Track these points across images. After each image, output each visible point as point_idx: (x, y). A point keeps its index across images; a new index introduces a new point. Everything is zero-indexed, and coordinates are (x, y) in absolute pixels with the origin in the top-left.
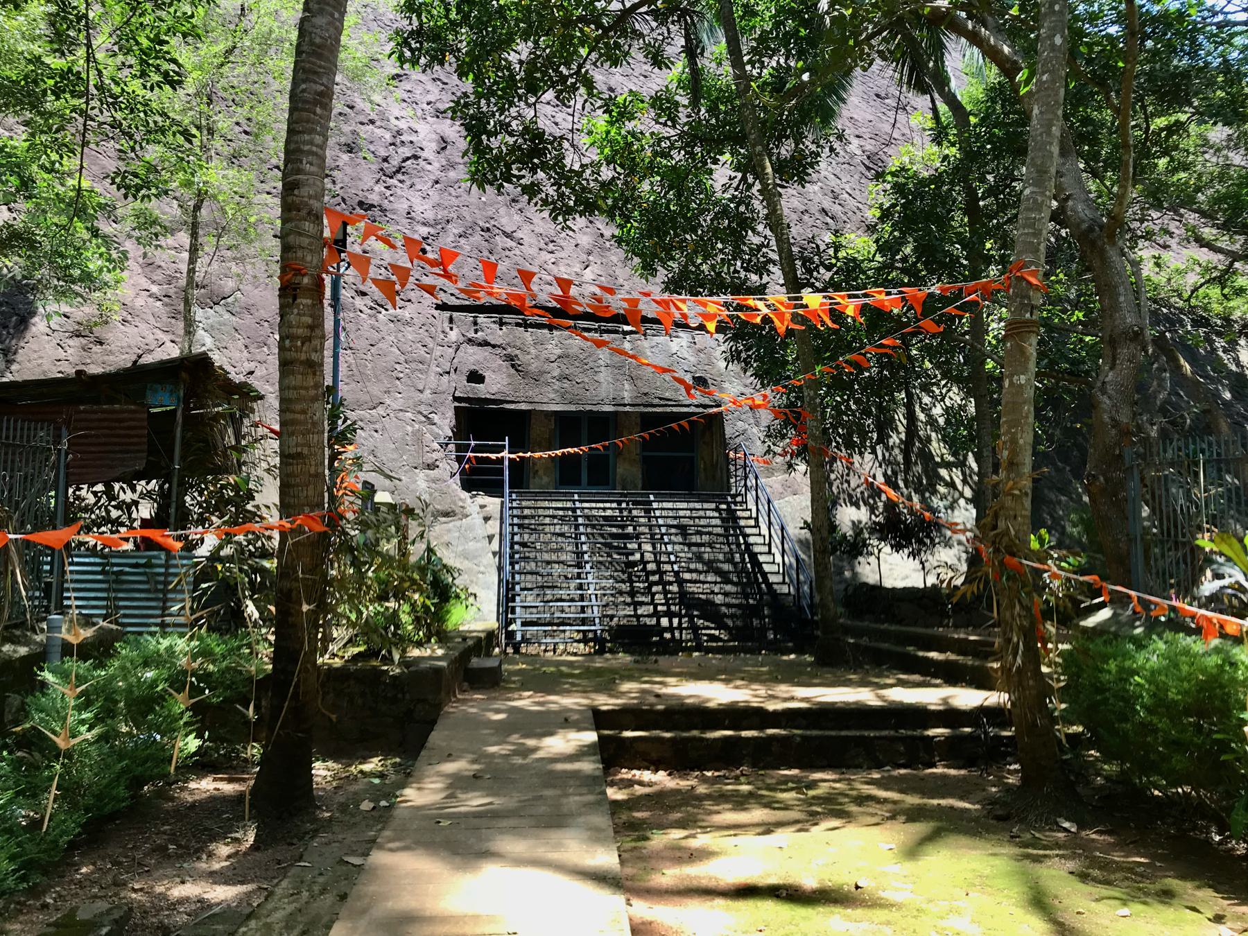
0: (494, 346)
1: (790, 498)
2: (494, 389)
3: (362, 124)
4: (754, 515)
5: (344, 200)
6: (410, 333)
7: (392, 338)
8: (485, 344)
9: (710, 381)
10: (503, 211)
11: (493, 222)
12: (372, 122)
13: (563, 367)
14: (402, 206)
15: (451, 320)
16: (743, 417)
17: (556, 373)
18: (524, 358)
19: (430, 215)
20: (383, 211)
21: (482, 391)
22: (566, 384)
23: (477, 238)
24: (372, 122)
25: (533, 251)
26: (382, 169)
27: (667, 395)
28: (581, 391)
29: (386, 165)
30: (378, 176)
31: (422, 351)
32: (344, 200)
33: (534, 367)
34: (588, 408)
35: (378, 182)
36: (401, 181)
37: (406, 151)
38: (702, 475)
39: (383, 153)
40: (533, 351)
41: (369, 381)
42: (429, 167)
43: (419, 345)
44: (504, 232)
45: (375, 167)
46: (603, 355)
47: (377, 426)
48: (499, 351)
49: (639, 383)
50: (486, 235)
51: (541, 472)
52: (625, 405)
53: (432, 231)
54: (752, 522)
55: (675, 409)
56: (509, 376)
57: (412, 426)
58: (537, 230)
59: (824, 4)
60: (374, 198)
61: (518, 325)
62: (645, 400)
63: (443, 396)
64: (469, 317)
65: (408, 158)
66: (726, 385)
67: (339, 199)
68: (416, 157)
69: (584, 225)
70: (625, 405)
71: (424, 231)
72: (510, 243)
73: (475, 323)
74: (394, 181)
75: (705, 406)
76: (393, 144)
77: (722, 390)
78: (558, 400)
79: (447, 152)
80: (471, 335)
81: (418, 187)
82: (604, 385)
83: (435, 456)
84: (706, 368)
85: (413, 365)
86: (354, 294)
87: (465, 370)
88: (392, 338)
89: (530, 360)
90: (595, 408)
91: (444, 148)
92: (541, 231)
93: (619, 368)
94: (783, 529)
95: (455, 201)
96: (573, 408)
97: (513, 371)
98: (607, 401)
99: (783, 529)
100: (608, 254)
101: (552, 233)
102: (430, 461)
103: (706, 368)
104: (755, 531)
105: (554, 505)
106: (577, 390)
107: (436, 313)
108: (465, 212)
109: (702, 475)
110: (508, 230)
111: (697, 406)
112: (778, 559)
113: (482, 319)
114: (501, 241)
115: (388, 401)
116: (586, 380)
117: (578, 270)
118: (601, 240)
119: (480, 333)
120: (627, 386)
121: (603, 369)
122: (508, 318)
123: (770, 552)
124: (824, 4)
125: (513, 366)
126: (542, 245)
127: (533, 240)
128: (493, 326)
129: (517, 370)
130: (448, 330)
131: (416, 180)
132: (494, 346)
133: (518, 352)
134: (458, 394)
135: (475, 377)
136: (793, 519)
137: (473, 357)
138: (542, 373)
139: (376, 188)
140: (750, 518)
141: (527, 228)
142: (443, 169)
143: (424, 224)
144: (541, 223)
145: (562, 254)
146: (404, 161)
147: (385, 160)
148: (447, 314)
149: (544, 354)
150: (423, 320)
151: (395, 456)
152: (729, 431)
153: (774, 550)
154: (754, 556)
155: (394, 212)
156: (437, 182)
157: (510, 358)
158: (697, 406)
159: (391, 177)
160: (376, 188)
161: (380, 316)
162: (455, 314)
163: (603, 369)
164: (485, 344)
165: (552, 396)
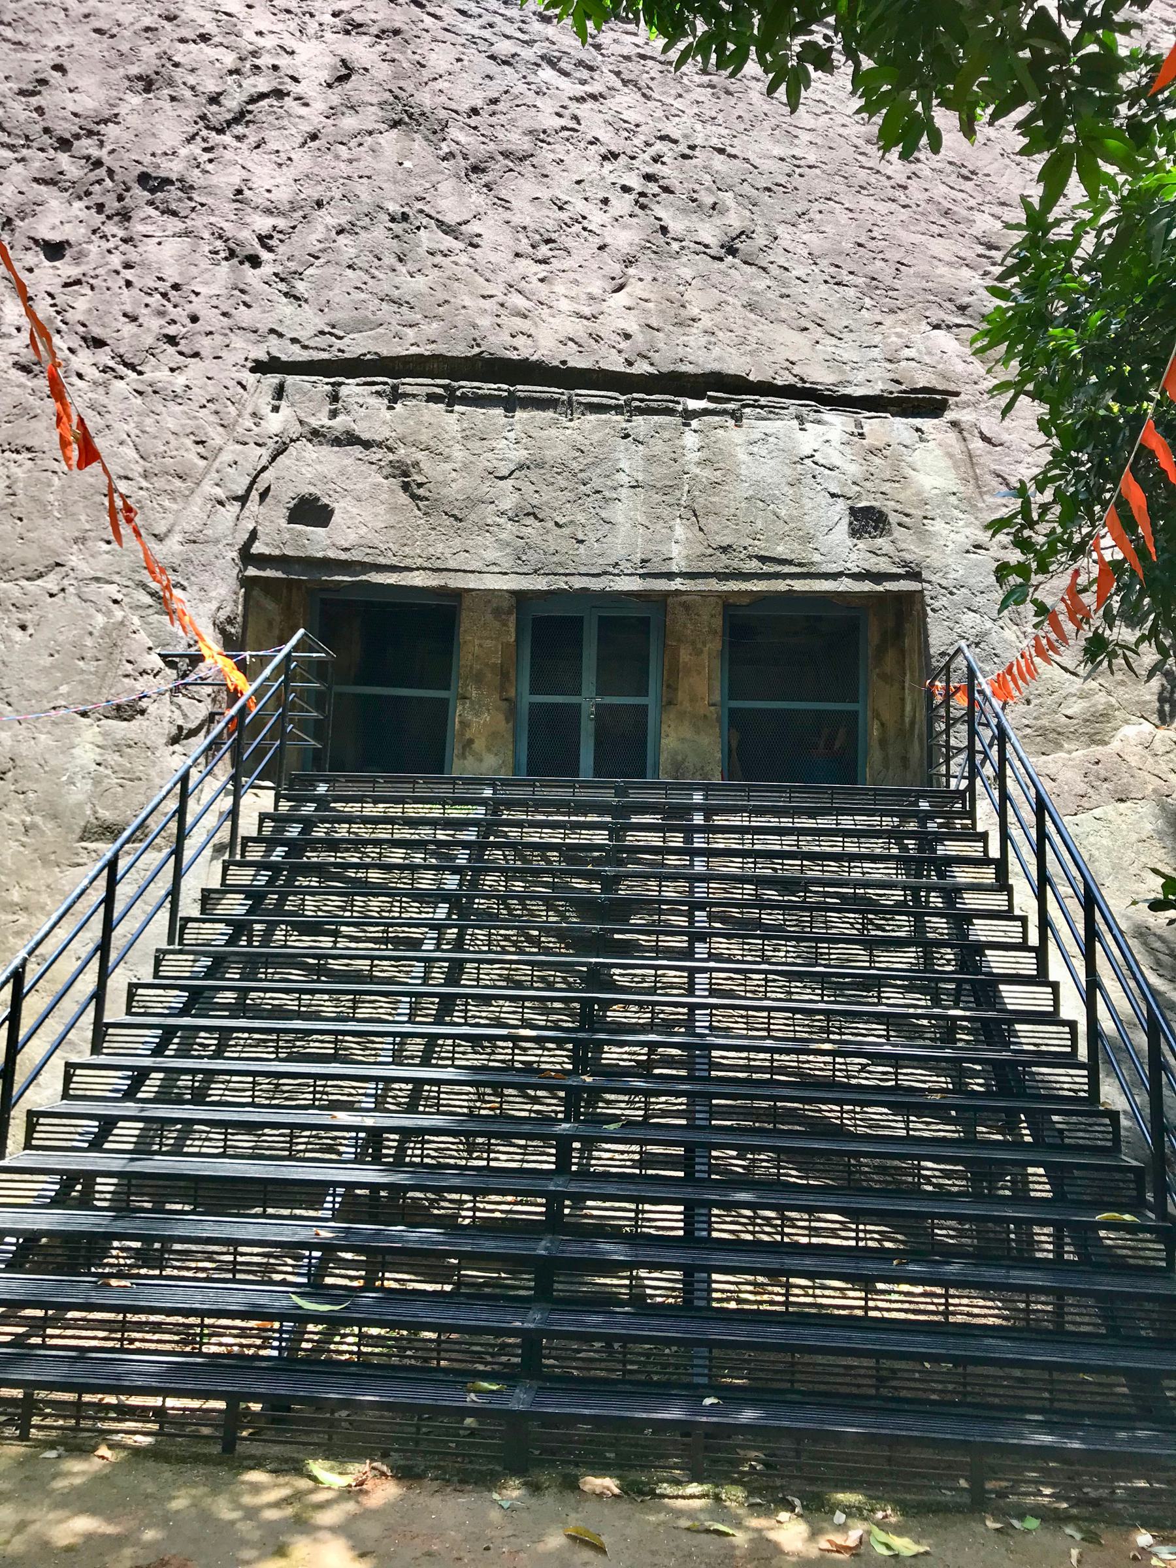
0: (367, 445)
1: (1110, 810)
2: (351, 538)
3: (183, 40)
4: (994, 852)
5: (111, 173)
6: (173, 417)
7: (130, 427)
8: (350, 439)
9: (893, 518)
10: (446, 187)
11: (419, 205)
12: (205, 38)
13: (528, 489)
14: (226, 178)
15: (280, 392)
16: (980, 601)
17: (508, 503)
18: (430, 468)
19: (282, 195)
20: (187, 188)
21: (318, 542)
22: (531, 529)
23: (379, 234)
24: (205, 38)
25: (502, 258)
26: (203, 117)
27: (780, 550)
28: (567, 545)
29: (214, 108)
30: (192, 130)
31: (191, 454)
32: (111, 173)
33: (456, 488)
34: (578, 583)
35: (191, 139)
36: (239, 138)
37: (263, 84)
38: (876, 755)
39: (212, 87)
40: (458, 454)
41: (46, 515)
42: (303, 111)
43: (188, 442)
44: (440, 224)
45: (189, 113)
46: (629, 462)
47: (27, 617)
48: (377, 454)
49: (711, 524)
50: (398, 228)
51: (479, 745)
52: (670, 576)
53: (282, 223)
54: (988, 875)
55: (799, 585)
56: (394, 509)
57: (109, 613)
58: (517, 220)
59: (1171, 114)
60: (172, 168)
61: (431, 398)
62: (722, 562)
63: (211, 550)
64: (323, 385)
65: (263, 96)
66: (938, 526)
67: (102, 172)
68: (279, 94)
69: (626, 211)
70: (670, 576)
71: (264, 224)
72: (448, 242)
73: (335, 398)
74: (227, 139)
75: (878, 577)
76: (237, 72)
77: (923, 536)
78: (506, 565)
79: (348, 86)
80: (320, 420)
81: (272, 145)
82: (623, 530)
83: (142, 684)
84: (886, 487)
85: (160, 483)
86: (76, 342)
87: (286, 494)
88: (130, 427)
89: (449, 478)
90: (595, 584)
91: (342, 79)
92: (527, 221)
93: (666, 490)
94: (1090, 901)
95: (344, 169)
96: (540, 584)
97: (404, 498)
98: (625, 566)
99: (1090, 901)
100: (673, 263)
101: (551, 225)
102: (123, 700)
103: (886, 487)
104: (997, 901)
105: (414, 810)
106: (555, 540)
107: (250, 379)
108: (362, 189)
109: (876, 755)
110: (451, 219)
111: (856, 577)
112: (1072, 1008)
113: (351, 388)
114: (430, 238)
115: (74, 560)
116: (581, 518)
117: (596, 290)
118: (660, 239)
119: (341, 418)
120: (680, 531)
121: (624, 493)
122: (409, 384)
123: (1041, 978)
124: (1171, 114)
125: (406, 487)
126: (524, 246)
127: (505, 238)
128: (374, 401)
129: (414, 497)
130: (266, 410)
131: (270, 135)
132: (367, 445)
133: (420, 456)
134: (258, 548)
135: (311, 511)
136: (1117, 868)
137: (310, 469)
138: (474, 502)
139: (183, 152)
140: (985, 861)
141: (496, 216)
142: (332, 113)
143: (268, 212)
144: (529, 208)
145: (567, 263)
146: (253, 100)
147: (214, 100)
148: (273, 379)
149: (486, 461)
150: (212, 389)
151: (43, 685)
152: (939, 637)
153: (1057, 970)
154: (985, 990)
155: (208, 190)
156: (314, 137)
157: (403, 473)
158: (856, 577)
159: (221, 131)
160: (183, 152)
161: (119, 385)
162: (291, 380)
163: (624, 493)
164: (350, 439)
165: (491, 555)
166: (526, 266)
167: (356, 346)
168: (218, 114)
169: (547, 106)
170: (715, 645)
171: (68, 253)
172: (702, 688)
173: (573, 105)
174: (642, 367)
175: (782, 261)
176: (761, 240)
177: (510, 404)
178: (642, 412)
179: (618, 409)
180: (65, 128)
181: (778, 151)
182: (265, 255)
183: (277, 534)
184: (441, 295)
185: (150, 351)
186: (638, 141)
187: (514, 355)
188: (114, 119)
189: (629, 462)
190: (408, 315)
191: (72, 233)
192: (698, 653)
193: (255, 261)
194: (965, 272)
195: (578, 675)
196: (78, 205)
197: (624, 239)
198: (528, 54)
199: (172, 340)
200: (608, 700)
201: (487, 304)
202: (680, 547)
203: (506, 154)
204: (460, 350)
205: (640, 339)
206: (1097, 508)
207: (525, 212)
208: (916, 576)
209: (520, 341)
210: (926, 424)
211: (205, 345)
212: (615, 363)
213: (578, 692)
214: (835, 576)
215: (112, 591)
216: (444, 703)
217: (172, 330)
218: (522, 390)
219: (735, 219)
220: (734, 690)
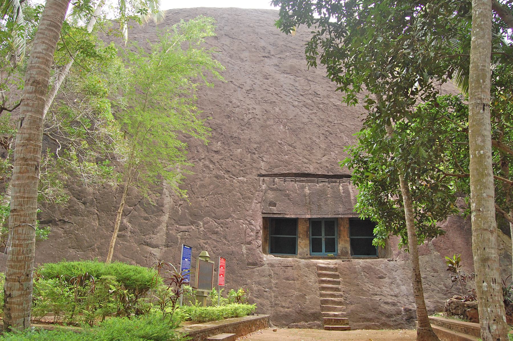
60: (235, 135)
64: (271, 179)
122: (288, 179)
125: (289, 199)
143: (255, 143)
162: (265, 178)
167: (276, 171)
169: (306, 116)
170: (347, 226)
172: (345, 235)
173: (310, 115)
174: (331, 174)
177: (308, 182)
187: (306, 172)
189: (329, 191)
192: (344, 228)
195: (334, 232)
197: (323, 146)
198: (300, 104)
200: (293, 236)
201: (300, 161)
209: (307, 169)
211: (248, 171)
213: (334, 235)
215: (242, 221)
216: (295, 238)
217: (242, 169)
220: (351, 234)
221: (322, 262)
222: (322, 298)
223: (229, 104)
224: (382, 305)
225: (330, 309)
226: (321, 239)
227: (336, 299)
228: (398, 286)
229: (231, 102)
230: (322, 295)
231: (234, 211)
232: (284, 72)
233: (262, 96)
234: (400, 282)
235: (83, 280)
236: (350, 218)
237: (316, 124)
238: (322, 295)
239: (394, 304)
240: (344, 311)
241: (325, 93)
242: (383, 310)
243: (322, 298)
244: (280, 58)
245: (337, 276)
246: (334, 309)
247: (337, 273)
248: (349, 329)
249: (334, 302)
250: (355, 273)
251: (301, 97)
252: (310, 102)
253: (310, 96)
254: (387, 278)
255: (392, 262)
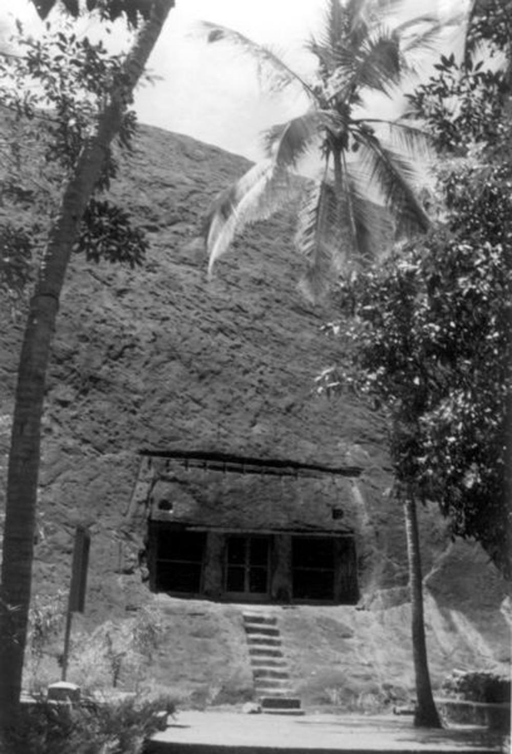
30: (105, 359)
37: (127, 342)
45: (103, 352)
62: (296, 526)
79: (156, 343)
113: (174, 462)
122: (192, 461)
147: (111, 347)
155: (115, 384)
166: (223, 417)
167: (174, 446)
168: (113, 353)
171: (70, 406)
174: (265, 458)
175: (306, 415)
176: (298, 407)
178: (267, 473)
179: (259, 472)
180: (60, 355)
181: (302, 369)
182: (137, 410)
183: (156, 513)
184: (198, 429)
185: (106, 446)
186: (254, 364)
188: (77, 353)
190: (190, 437)
191: (69, 398)
193: (134, 412)
194: (365, 422)
196: (69, 387)
197: (255, 405)
199: (111, 442)
202: (283, 522)
203: (212, 372)
204: (207, 450)
205: (265, 447)
206: (488, 410)
207: (220, 396)
208: (352, 532)
210: (354, 479)
212: (256, 456)
214: (329, 532)
218: (228, 464)
219: (289, 399)
221: (250, 610)
222: (256, 668)
223: (88, 314)
224: (349, 679)
225: (267, 685)
226: (243, 569)
227: (277, 669)
228: (372, 650)
229: (89, 311)
230: (254, 663)
231: (99, 515)
232: (184, 261)
233: (146, 305)
234: (375, 645)
235: (194, 615)
236: (226, 535)
237: (240, 366)
238: (254, 663)
239: (367, 678)
240: (290, 687)
241: (258, 311)
242: (351, 687)
243: (256, 668)
244: (176, 233)
245: (275, 633)
246: (274, 685)
247: (275, 627)
248: (301, 714)
249: (274, 674)
250: (306, 627)
251: (214, 314)
252: (231, 323)
253: (231, 314)
254: (355, 637)
255: (362, 612)
